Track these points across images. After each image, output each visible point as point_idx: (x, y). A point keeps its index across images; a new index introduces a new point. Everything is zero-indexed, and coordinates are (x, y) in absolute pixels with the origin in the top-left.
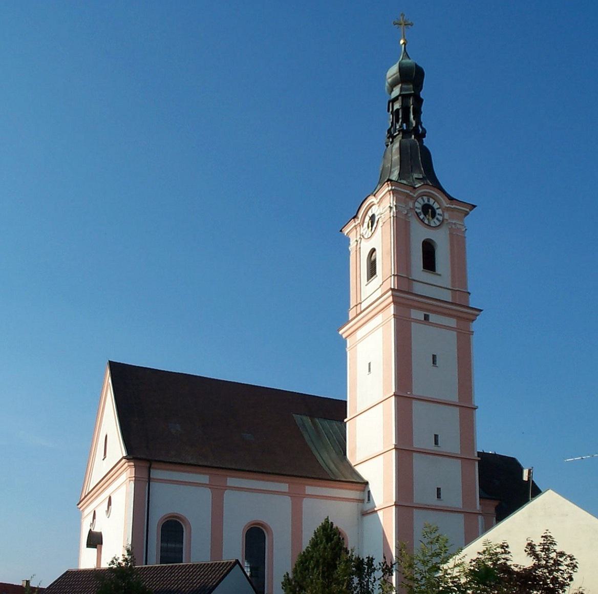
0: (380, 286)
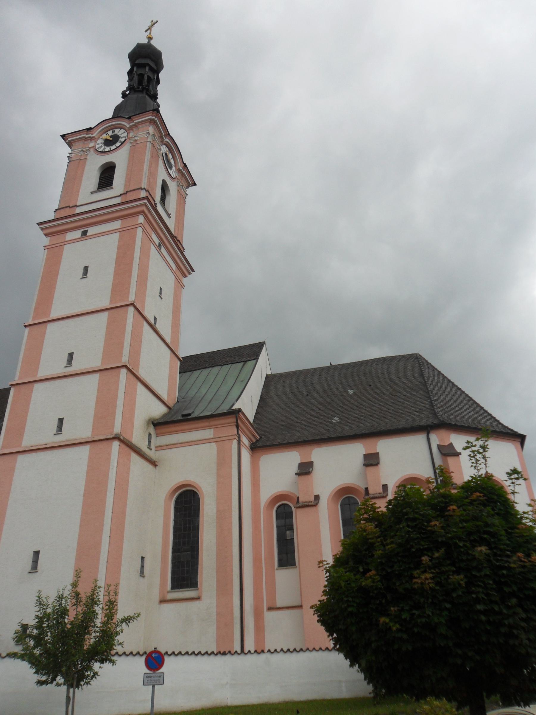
0: (121, 195)
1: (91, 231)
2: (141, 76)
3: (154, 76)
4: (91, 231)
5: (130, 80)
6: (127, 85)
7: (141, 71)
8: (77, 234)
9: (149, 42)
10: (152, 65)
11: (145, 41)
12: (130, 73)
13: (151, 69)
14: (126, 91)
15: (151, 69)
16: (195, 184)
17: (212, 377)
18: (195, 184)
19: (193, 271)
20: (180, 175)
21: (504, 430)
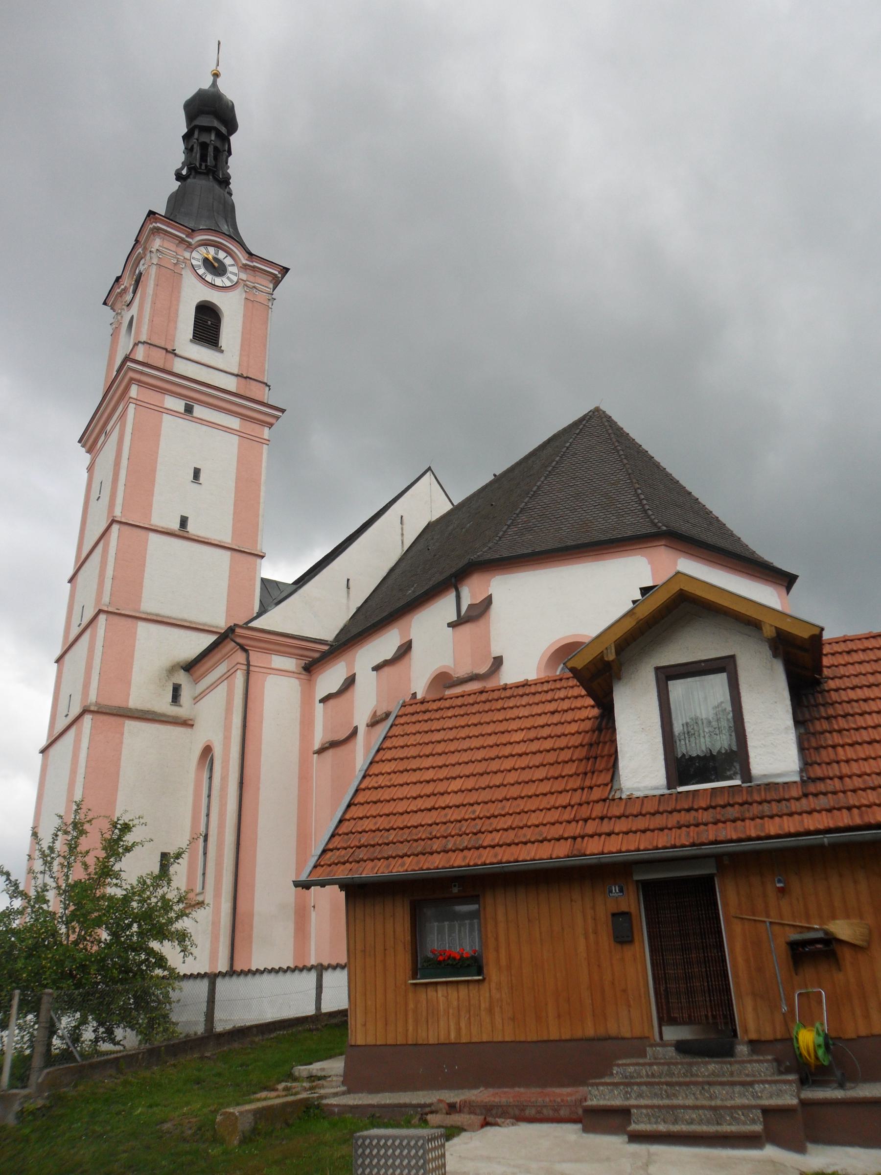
1: (199, 411)
2: (204, 146)
3: (224, 145)
4: (199, 411)
5: (189, 150)
6: (182, 157)
7: (205, 138)
8: (179, 405)
9: (214, 84)
10: (223, 130)
11: (206, 85)
12: (186, 137)
13: (219, 134)
14: (182, 168)
15: (219, 134)
16: (286, 270)
17: (578, 703)
18: (286, 270)
19: (283, 411)
20: (314, 1073)
21: (738, 550)
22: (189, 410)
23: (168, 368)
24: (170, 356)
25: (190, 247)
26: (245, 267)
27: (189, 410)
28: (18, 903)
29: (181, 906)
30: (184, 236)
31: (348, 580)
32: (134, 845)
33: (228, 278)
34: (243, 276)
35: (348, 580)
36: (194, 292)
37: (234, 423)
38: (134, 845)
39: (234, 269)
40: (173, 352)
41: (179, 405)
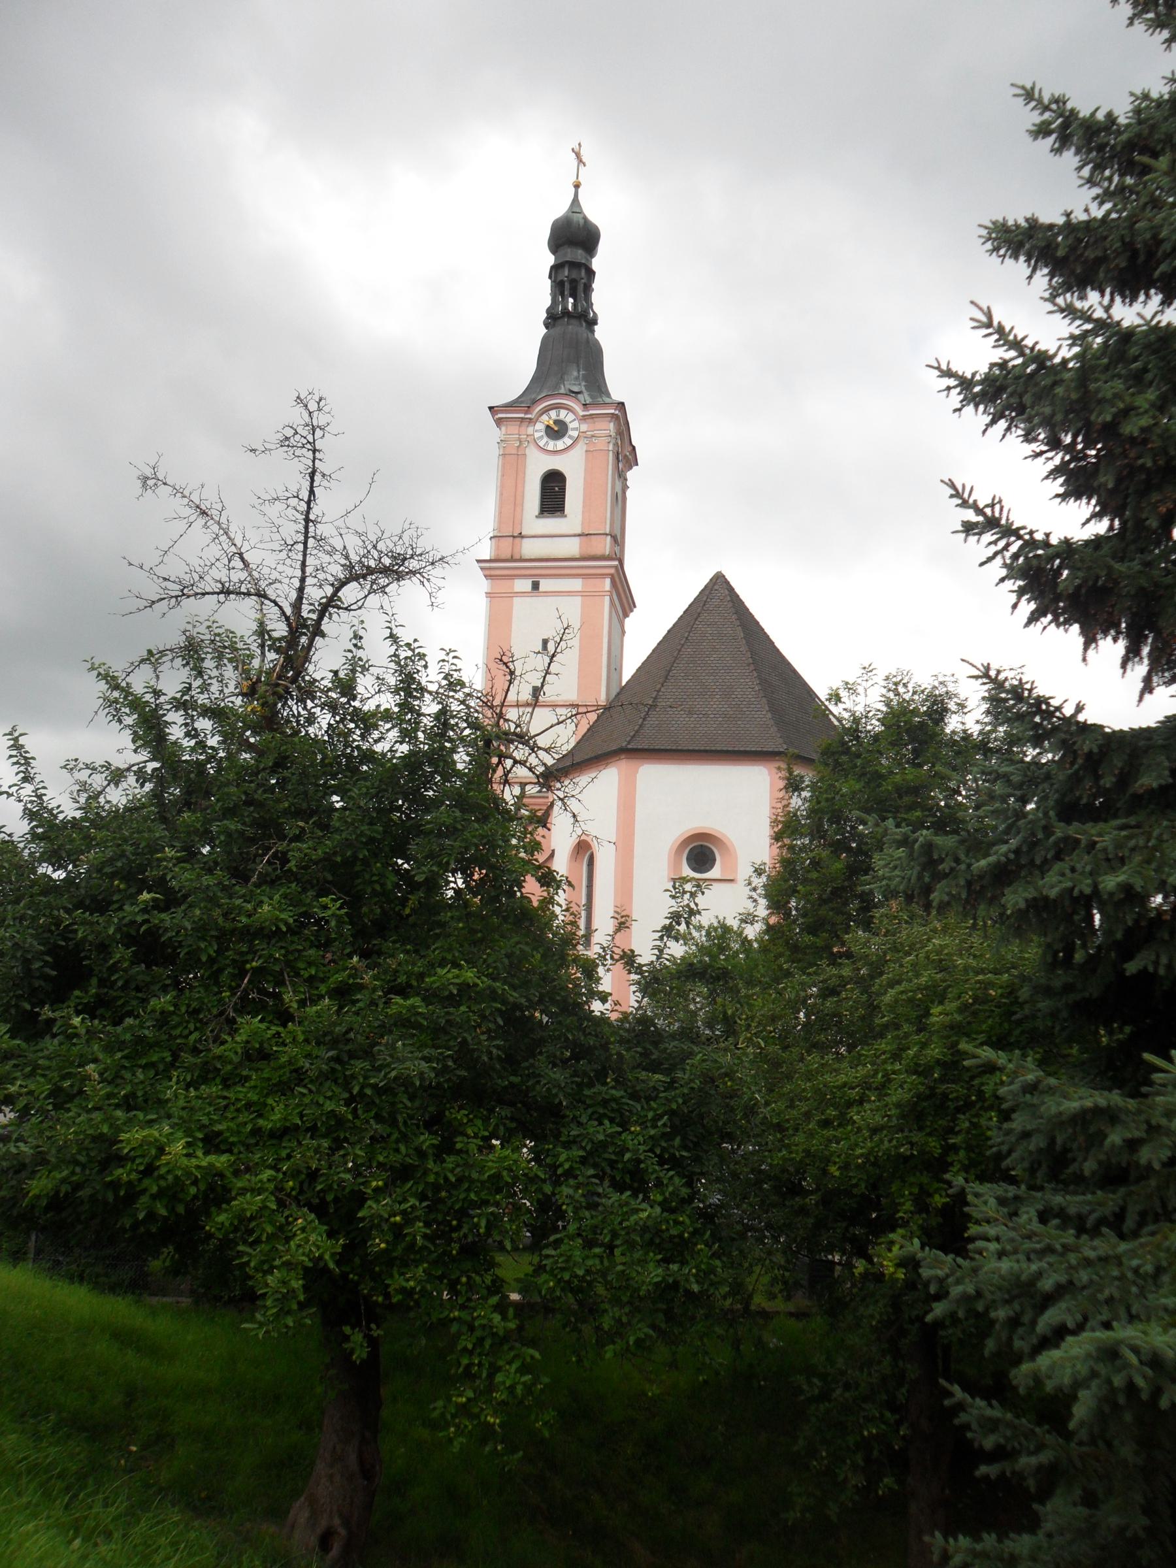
1: (545, 585)
22: (536, 586)
23: (517, 556)
24: (518, 540)
25: (531, 421)
26: (584, 418)
27: (536, 586)
28: (1047, 115)
29: (1100, 1443)
30: (522, 415)
31: (982, 564)
32: (217, 581)
33: (573, 429)
34: (584, 427)
35: (982, 564)
36: (537, 466)
37: (576, 584)
38: (217, 581)
39: (575, 424)
40: (521, 536)
41: (525, 585)
